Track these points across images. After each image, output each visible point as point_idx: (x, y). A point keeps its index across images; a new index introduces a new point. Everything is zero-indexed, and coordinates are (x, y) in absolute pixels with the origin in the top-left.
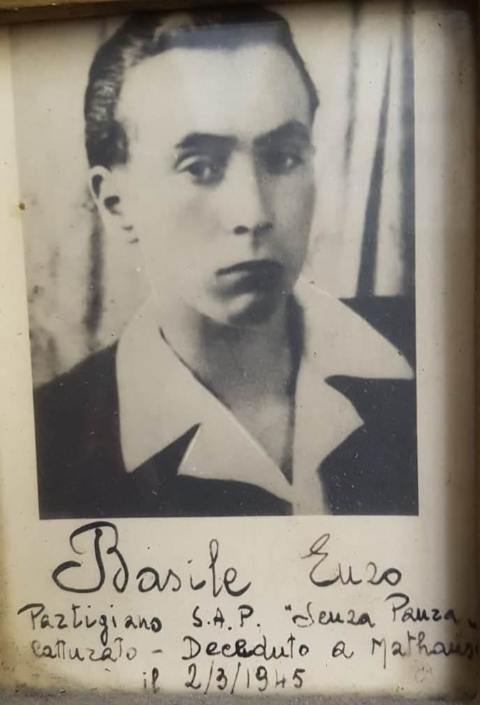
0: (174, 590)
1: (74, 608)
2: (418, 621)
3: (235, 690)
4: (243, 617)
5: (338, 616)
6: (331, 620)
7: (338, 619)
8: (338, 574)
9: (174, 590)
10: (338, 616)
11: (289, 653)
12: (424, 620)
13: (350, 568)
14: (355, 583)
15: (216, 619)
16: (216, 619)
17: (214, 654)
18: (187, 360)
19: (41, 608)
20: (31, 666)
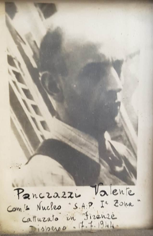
1: (53, 216)
4: (90, 206)
7: (49, 220)
11: (80, 224)
16: (83, 206)
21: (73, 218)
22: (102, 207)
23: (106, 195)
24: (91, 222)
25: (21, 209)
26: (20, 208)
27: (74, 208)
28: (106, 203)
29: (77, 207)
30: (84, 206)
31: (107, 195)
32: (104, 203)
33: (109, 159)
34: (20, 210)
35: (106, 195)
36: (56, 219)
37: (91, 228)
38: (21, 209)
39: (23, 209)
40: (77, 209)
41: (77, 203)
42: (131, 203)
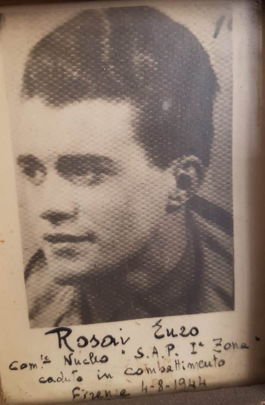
0: (132, 369)
2: (34, 364)
3: (213, 28)
5: (210, 363)
6: (205, 365)
7: (210, 365)
8: (170, 351)
9: (132, 369)
10: (210, 363)
12: (78, 364)
13: (169, 355)
14: (174, 336)
15: (154, 353)
16: (154, 353)
17: (167, 346)
18: (143, 388)
19: (12, 367)
20: (5, 248)
21: (154, 371)
22: (194, 353)
23: (113, 344)
24: (70, 380)
25: (35, 365)
26: (171, 336)
27: (136, 357)
28: (201, 344)
29: (142, 355)
30: (157, 353)
31: (115, 344)
32: (197, 347)
33: (137, 74)
34: (33, 366)
35: (113, 344)
36: (221, 364)
37: (174, 384)
38: (35, 365)
39: (39, 363)
40: (142, 359)
41: (141, 348)
42: (170, 367)
